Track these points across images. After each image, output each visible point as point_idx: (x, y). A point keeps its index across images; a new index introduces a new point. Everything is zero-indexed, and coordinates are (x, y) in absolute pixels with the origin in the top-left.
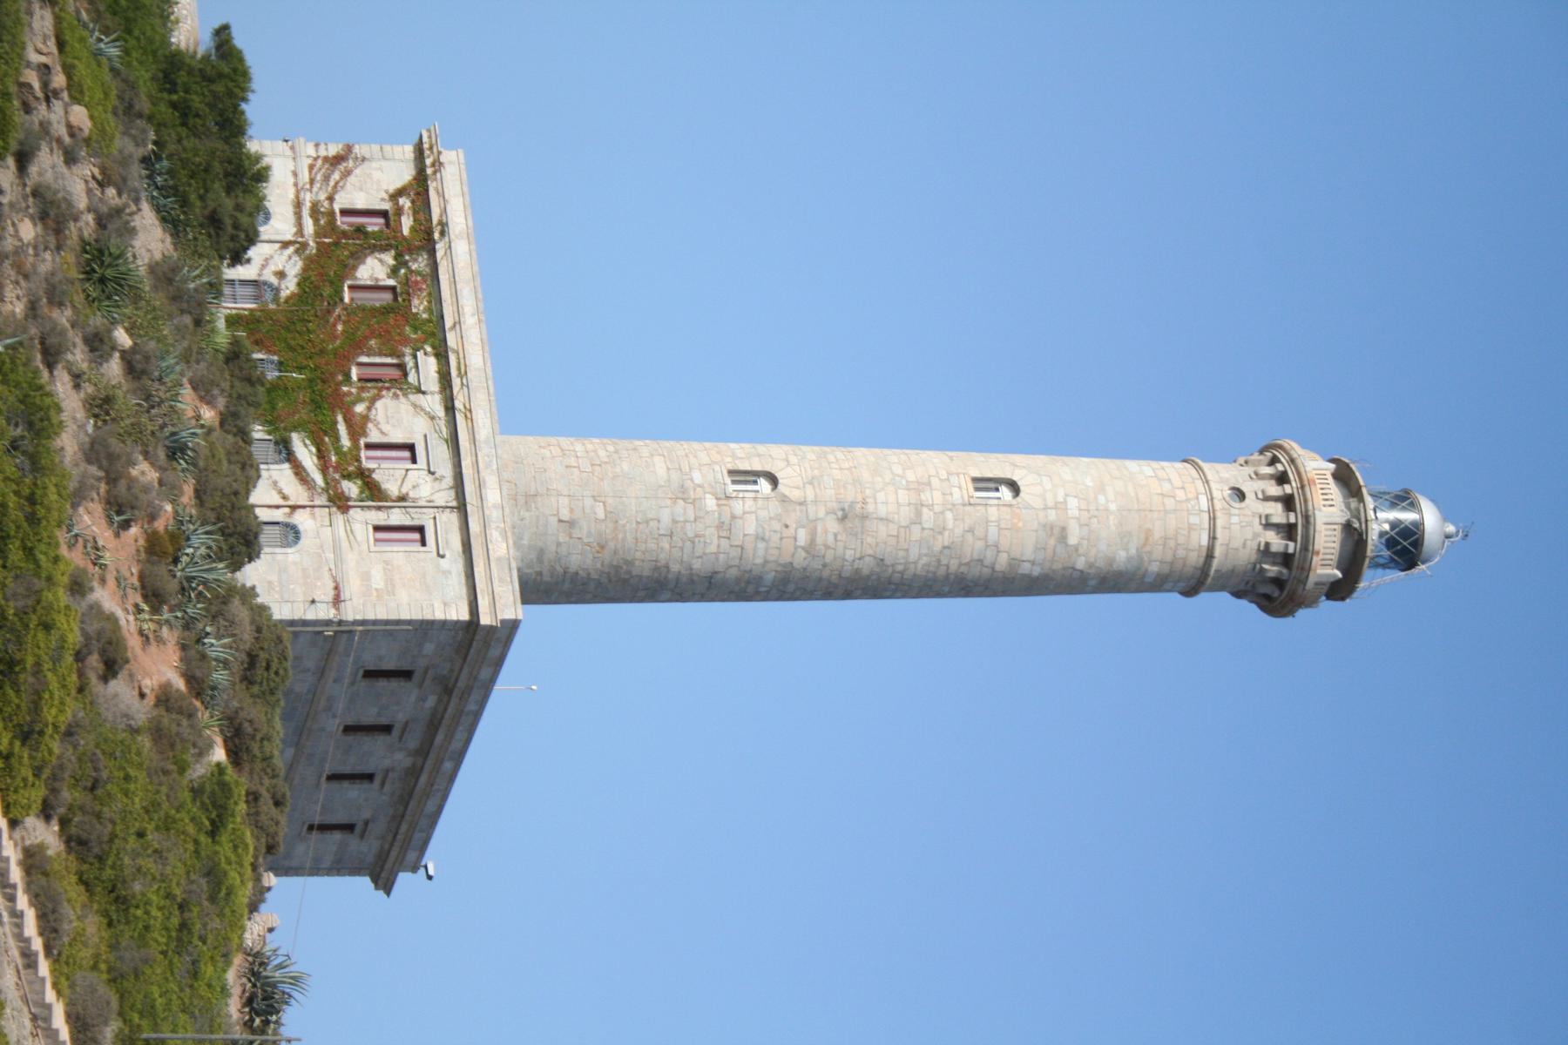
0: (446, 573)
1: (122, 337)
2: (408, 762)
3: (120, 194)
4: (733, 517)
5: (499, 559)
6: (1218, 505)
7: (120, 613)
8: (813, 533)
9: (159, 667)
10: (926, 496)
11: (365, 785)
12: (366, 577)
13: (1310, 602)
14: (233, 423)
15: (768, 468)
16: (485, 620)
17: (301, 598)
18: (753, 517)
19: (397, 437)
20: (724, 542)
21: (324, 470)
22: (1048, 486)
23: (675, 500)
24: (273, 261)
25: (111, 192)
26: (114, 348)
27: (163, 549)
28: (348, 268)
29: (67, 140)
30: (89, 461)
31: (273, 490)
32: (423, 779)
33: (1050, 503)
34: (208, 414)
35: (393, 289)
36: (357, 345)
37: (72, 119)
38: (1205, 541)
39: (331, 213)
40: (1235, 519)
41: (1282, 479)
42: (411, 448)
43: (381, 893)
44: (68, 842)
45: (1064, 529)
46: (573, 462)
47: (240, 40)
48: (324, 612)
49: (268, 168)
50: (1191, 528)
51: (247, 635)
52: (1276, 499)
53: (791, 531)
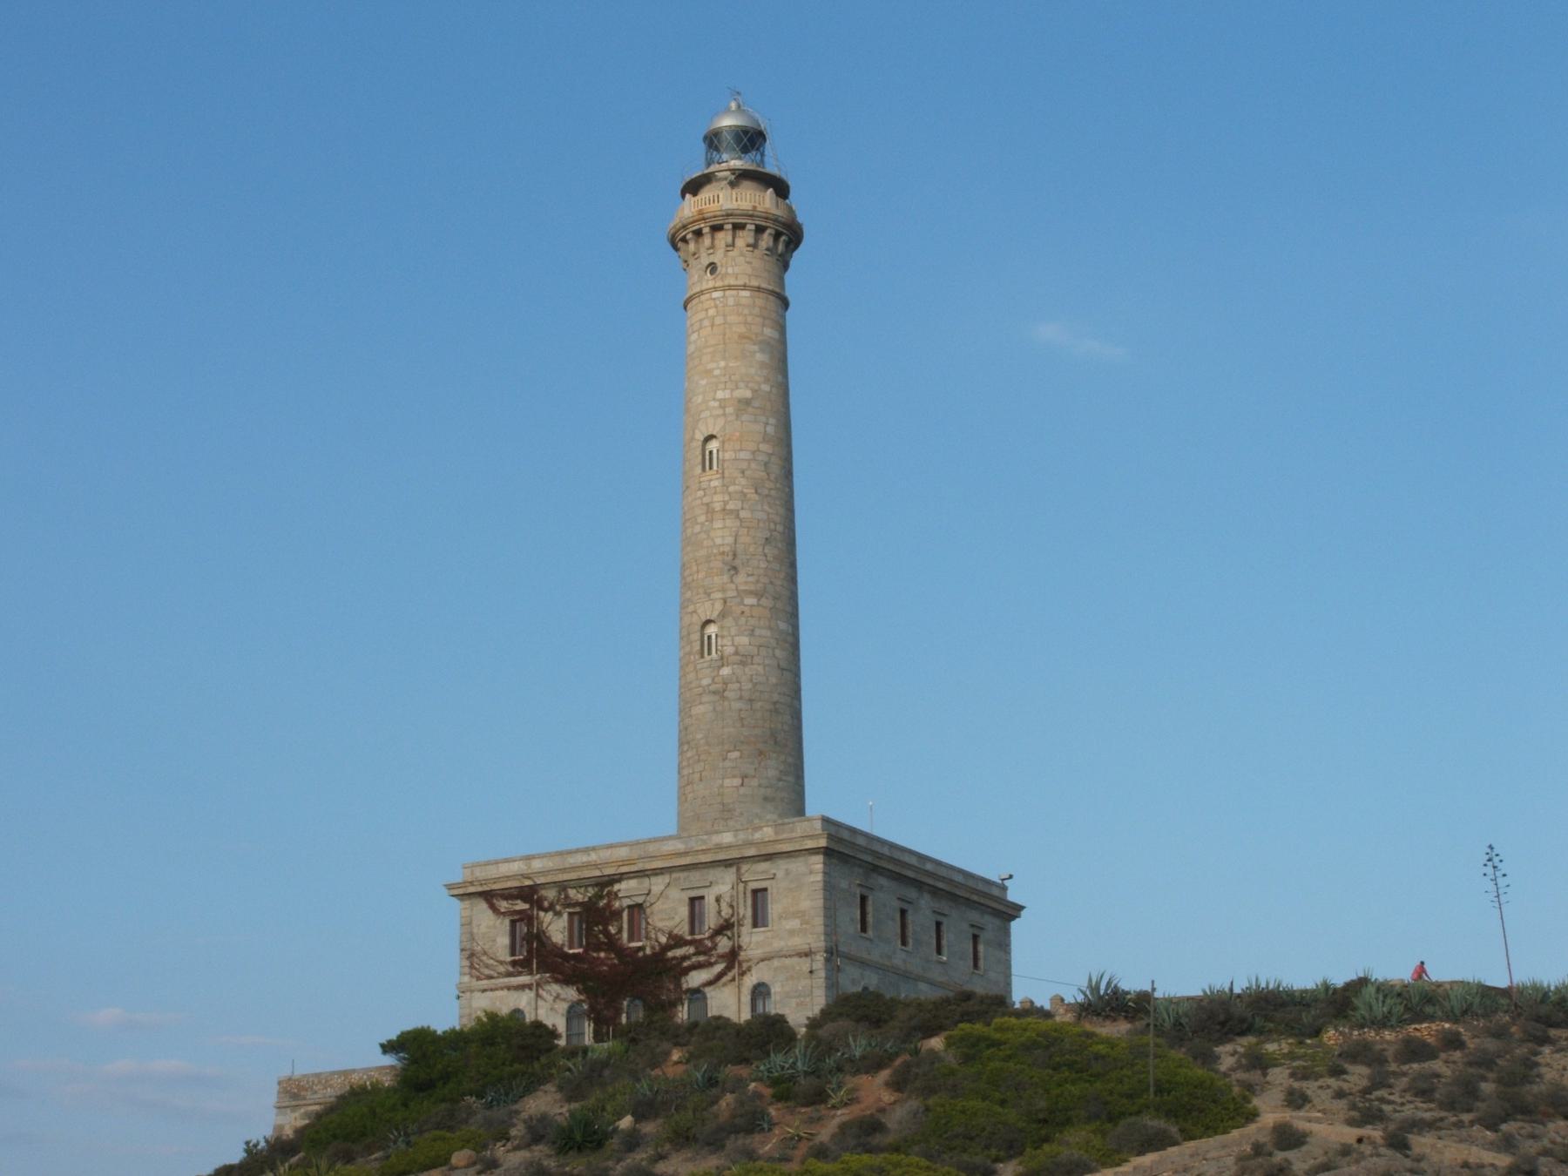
0: (787, 873)
1: (626, 1122)
2: (927, 896)
3: (514, 1125)
4: (736, 653)
5: (776, 833)
6: (719, 284)
7: (836, 1122)
8: (751, 593)
9: (874, 1090)
10: (718, 506)
11: (944, 928)
12: (792, 933)
13: (790, 209)
14: (678, 1036)
15: (698, 628)
16: (823, 843)
17: (808, 982)
18: (737, 639)
19: (684, 911)
20: (756, 659)
21: (710, 965)
22: (707, 413)
23: (724, 698)
24: (549, 1006)
25: (513, 1132)
26: (634, 1129)
27: (784, 1090)
28: (558, 951)
29: (478, 1167)
30: (723, 1147)
31: (729, 1003)
32: (940, 885)
33: (720, 412)
34: (676, 1055)
35: (570, 914)
36: (612, 944)
37: (462, 1164)
38: (746, 293)
39: (514, 963)
40: (730, 270)
41: (698, 233)
42: (692, 900)
43: (1023, 913)
44: (1010, 1157)
45: (740, 401)
46: (697, 776)
47: (393, 1035)
48: (819, 961)
49: (487, 1013)
50: (738, 305)
51: (843, 1023)
52: (713, 238)
53: (746, 609)
